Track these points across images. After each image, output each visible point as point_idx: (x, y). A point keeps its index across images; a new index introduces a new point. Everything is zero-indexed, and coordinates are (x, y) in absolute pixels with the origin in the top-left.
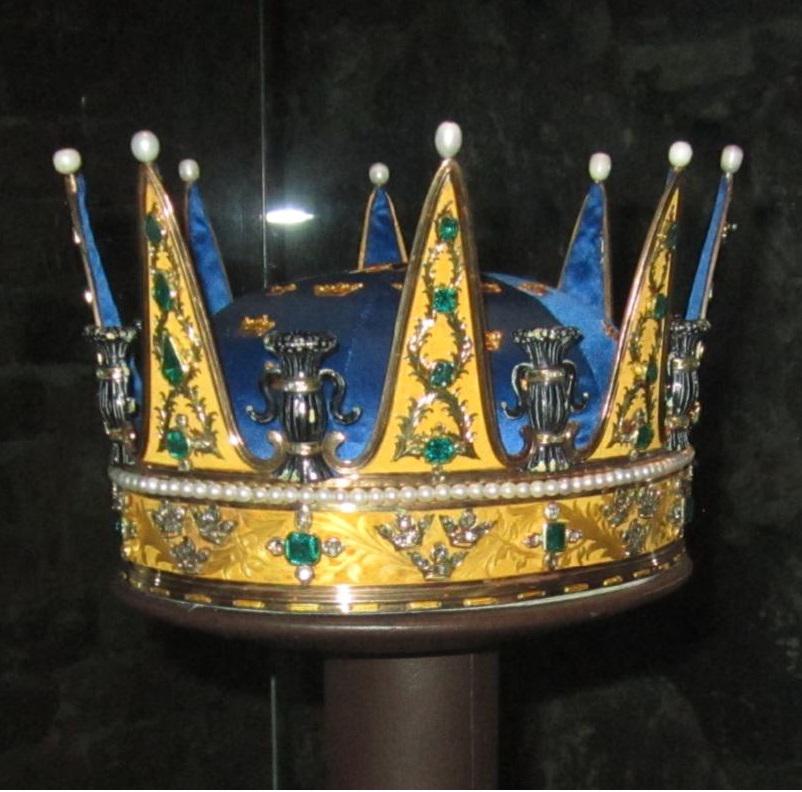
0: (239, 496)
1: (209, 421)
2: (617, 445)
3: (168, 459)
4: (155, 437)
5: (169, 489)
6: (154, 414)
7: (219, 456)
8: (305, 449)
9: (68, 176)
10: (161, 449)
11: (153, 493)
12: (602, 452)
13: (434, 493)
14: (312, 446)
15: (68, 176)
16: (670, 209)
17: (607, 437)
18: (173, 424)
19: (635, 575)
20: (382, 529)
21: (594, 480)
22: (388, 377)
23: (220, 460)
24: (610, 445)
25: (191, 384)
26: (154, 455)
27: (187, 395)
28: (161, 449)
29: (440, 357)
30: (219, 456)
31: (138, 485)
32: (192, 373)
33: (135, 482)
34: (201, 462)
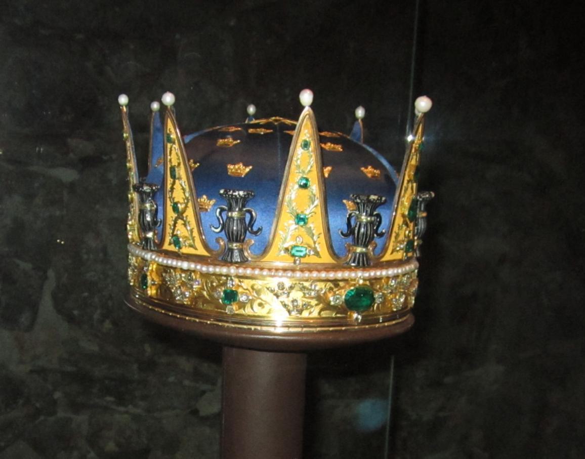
0: (220, 269)
1: (192, 231)
2: (395, 253)
3: (172, 248)
4: (168, 238)
5: (172, 263)
6: (168, 227)
7: (196, 249)
8: (235, 246)
9: (122, 106)
10: (170, 244)
11: (325, 279)
12: (388, 257)
13: (319, 275)
14: (156, 112)
15: (122, 106)
16: (418, 133)
17: (389, 251)
18: (175, 233)
19: (155, 237)
20: (283, 303)
21: (381, 273)
22: (282, 187)
23: (196, 251)
24: (392, 253)
25: (184, 215)
26: (166, 246)
27: (182, 219)
28: (170, 244)
29: (306, 190)
30: (196, 249)
31: (144, 256)
32: (184, 211)
33: (140, 253)
34: (185, 250)
